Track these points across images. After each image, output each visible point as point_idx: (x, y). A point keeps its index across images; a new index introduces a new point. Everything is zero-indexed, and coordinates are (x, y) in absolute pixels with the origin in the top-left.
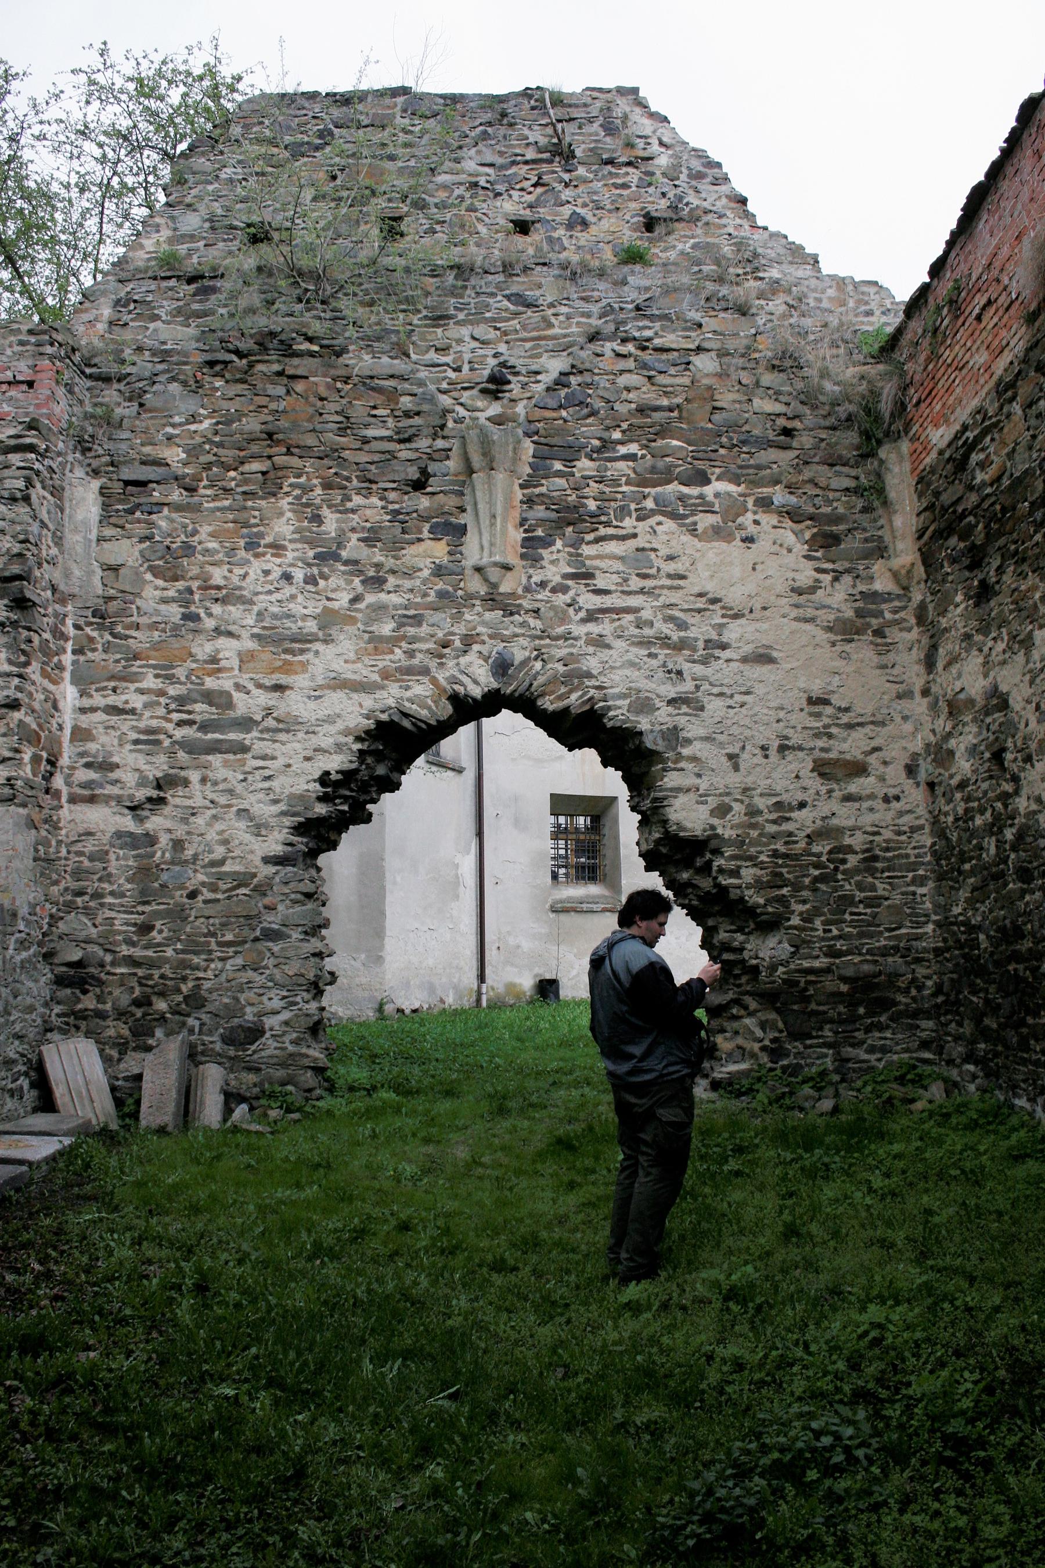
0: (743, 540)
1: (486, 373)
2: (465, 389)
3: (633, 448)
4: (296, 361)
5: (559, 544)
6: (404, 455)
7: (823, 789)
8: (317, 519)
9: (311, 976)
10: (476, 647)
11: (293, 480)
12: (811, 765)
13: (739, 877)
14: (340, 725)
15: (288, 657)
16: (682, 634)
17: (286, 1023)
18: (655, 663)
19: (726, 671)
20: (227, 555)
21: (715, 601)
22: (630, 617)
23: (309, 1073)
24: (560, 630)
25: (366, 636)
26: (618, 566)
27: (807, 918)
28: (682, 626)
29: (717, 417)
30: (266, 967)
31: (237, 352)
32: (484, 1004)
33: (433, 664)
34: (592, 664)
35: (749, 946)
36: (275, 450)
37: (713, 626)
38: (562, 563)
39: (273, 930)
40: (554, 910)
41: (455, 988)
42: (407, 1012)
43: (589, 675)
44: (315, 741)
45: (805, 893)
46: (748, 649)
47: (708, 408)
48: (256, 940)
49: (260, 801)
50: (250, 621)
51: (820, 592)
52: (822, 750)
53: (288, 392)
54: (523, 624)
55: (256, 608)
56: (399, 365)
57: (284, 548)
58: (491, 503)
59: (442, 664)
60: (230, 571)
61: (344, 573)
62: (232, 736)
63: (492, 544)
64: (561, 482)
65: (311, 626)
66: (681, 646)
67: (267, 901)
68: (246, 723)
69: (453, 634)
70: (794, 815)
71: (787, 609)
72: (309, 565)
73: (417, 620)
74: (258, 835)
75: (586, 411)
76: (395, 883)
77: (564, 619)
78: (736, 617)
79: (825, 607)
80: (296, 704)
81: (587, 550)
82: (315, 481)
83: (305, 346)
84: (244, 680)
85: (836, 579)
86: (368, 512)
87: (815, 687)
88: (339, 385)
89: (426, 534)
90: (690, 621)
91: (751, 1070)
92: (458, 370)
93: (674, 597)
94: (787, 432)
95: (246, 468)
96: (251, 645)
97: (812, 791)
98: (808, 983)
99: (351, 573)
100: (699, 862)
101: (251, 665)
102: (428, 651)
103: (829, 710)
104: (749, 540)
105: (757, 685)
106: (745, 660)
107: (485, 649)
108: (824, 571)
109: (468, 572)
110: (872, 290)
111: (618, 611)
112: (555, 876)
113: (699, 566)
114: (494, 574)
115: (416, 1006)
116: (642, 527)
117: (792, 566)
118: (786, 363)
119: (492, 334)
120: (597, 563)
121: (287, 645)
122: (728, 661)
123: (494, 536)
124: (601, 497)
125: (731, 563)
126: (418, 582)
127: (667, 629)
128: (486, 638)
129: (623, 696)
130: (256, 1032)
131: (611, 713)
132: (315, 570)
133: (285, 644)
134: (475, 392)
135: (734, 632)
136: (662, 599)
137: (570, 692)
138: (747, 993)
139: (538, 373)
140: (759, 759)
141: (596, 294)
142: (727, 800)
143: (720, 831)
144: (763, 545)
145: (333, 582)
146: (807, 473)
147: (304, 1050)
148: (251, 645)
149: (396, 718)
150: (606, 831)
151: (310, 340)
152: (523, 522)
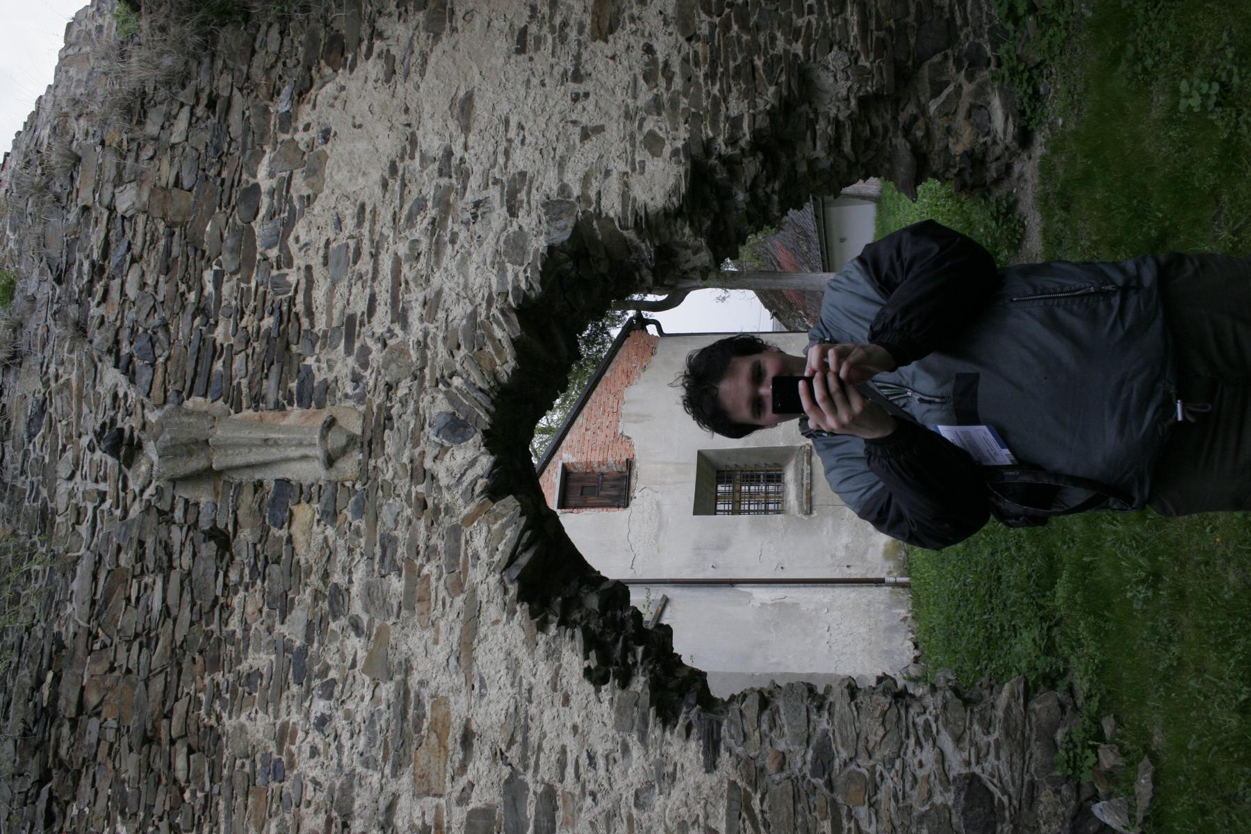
0: (326, 141)
1: (110, 460)
2: (125, 487)
3: (208, 276)
4: (62, 702)
5: (310, 361)
6: (186, 561)
7: (630, 27)
8: (253, 677)
9: (885, 701)
10: (428, 464)
11: (202, 712)
12: (600, 44)
13: (739, 118)
14: (521, 652)
15: (425, 725)
16: (430, 204)
17: (958, 740)
18: (463, 235)
19: (478, 149)
20: (286, 808)
21: (393, 169)
22: (405, 269)
23: (1035, 705)
25: (404, 613)
26: (342, 288)
27: (794, 34)
28: (421, 205)
29: (187, 183)
30: (872, 770)
31: (41, 782)
32: (906, 579)
33: (446, 521)
34: (459, 312)
35: (833, 112)
36: (163, 734)
38: (332, 356)
39: (815, 760)
40: (809, 512)
41: (890, 607)
42: (917, 653)
43: (473, 316)
44: (541, 690)
45: (762, 38)
46: (453, 125)
47: (175, 191)
48: (830, 785)
49: (625, 773)
50: (375, 778)
51: (393, 51)
52: (581, 32)
53: (98, 714)
55: (359, 769)
56: (84, 569)
57: (285, 726)
58: (250, 446)
59: (448, 510)
60: (309, 803)
61: (321, 644)
62: (531, 811)
63: (300, 444)
64: (239, 361)
65: (387, 690)
66: (444, 206)
67: (771, 767)
68: (513, 788)
69: (409, 493)
70: (661, 58)
71: (410, 86)
72: (309, 691)
73: (388, 543)
74: (673, 777)
75: (161, 335)
76: (778, 664)
77: (402, 351)
78: (413, 141)
79: (411, 44)
80: (490, 715)
81: (321, 325)
82: (207, 681)
83: (45, 690)
84: (454, 790)
85: (380, 35)
86: (250, 609)
87: (505, 46)
88: (97, 646)
89: (283, 533)
90: (415, 195)
91: (1001, 89)
92: (103, 496)
93: (385, 215)
94: (211, 105)
95: (181, 775)
96: (406, 779)
97: (632, 40)
98: (879, 28)
99: (323, 632)
100: (721, 174)
101: (433, 778)
102: (429, 528)
103: (533, 29)
104: (326, 135)
105: (498, 113)
106: (466, 129)
107: (431, 452)
109: (334, 475)
110: (76, 28)
111: (396, 282)
112: (778, 512)
113: (350, 189)
114: (336, 440)
115: (910, 644)
116: (299, 261)
117: (360, 83)
118: (136, 107)
119: (69, 455)
120: (336, 313)
121: (409, 726)
122: (466, 148)
123: (289, 443)
124: (259, 313)
125: (351, 153)
126: (341, 542)
127: (422, 223)
128: (417, 451)
129: (502, 271)
130: (973, 788)
131: (523, 286)
132: (316, 683)
133: (407, 729)
134: (130, 474)
135: (431, 144)
136: (386, 231)
137: (492, 337)
138: (895, 118)
139: (115, 396)
140: (590, 104)
141: (40, 332)
142: (639, 138)
143: (680, 144)
144: (334, 118)
145: (332, 659)
146: (257, 74)
147: (1000, 713)
148: (406, 779)
149: (515, 572)
150: (732, 464)
151: (40, 682)
152: (279, 407)
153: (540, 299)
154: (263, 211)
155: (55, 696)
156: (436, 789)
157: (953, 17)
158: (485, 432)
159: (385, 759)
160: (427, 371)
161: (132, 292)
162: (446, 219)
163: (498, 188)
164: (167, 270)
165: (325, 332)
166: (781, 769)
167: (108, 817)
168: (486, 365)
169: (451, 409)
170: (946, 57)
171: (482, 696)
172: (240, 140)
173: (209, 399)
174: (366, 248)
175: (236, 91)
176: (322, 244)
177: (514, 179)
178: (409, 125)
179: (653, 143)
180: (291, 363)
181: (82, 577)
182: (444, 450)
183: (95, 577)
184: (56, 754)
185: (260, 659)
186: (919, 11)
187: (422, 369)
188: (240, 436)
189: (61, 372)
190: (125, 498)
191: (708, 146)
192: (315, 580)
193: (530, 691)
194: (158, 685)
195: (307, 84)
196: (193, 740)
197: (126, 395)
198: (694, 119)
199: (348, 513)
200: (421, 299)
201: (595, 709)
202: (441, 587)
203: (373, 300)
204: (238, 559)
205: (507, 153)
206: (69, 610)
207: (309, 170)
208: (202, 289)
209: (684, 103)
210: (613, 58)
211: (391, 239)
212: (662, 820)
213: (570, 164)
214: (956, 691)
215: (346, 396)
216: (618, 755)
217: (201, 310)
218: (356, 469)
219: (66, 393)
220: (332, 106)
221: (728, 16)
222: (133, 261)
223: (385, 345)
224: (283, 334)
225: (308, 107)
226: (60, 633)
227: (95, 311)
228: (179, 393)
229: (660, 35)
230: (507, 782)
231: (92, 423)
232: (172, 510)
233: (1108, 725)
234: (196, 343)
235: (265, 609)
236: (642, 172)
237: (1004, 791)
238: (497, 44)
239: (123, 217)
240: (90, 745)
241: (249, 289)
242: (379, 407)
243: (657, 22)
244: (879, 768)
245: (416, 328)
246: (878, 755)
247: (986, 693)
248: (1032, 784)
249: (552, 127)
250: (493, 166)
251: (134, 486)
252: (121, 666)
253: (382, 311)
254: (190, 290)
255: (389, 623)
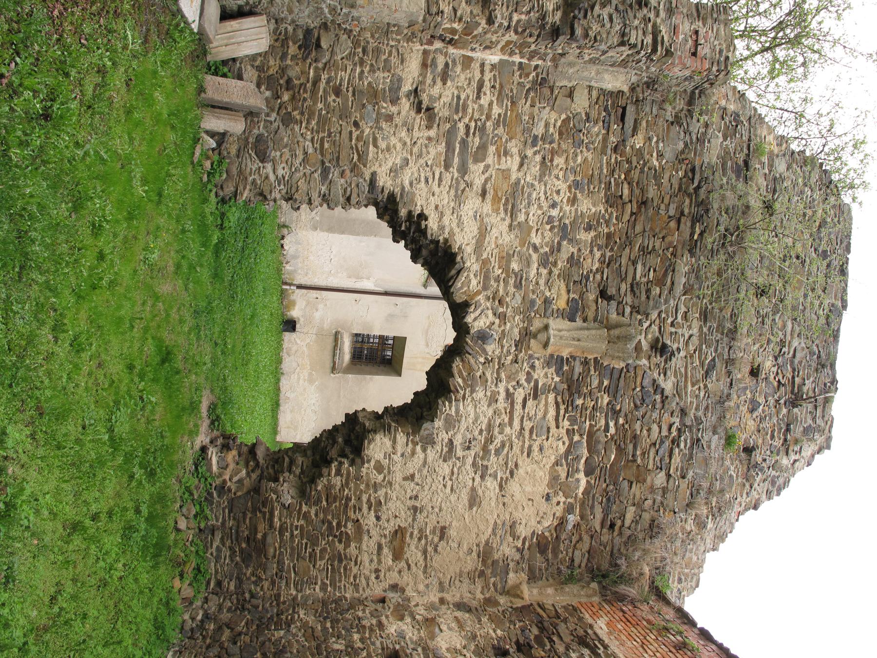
1: (668, 342)
3: (612, 430)
4: (689, 224)
5: (557, 379)
6: (623, 286)
7: (387, 532)
8: (589, 228)
9: (296, 196)
10: (497, 321)
14: (456, 230)
16: (493, 452)
17: (267, 177)
18: (476, 433)
20: (572, 168)
21: (512, 473)
22: (507, 420)
24: (503, 376)
26: (540, 415)
27: (306, 516)
28: (498, 452)
29: (626, 482)
30: (305, 168)
31: (699, 187)
32: (285, 287)
33: (489, 293)
34: (480, 394)
35: (291, 477)
36: (635, 206)
37: (496, 472)
38: (545, 380)
40: (337, 333)
41: (295, 271)
42: (282, 242)
44: (448, 212)
46: (480, 492)
48: (323, 163)
51: (511, 539)
52: (412, 533)
53: (670, 217)
54: (509, 352)
55: (536, 183)
56: (679, 289)
57: (573, 205)
59: (488, 298)
60: (561, 169)
61: (553, 241)
62: (456, 160)
64: (595, 383)
65: (521, 218)
67: (348, 172)
68: (463, 170)
69: (507, 308)
72: (560, 220)
73: (518, 286)
77: (509, 378)
80: (472, 204)
81: (551, 397)
82: (612, 229)
84: (492, 171)
85: (518, 550)
86: (590, 260)
87: (451, 532)
88: (671, 249)
89: (572, 296)
90: (501, 458)
92: (672, 325)
93: (516, 450)
94: (612, 526)
95: (626, 186)
96: (514, 177)
97: (386, 525)
98: (264, 513)
101: (501, 177)
103: (436, 539)
104: (548, 498)
106: (473, 489)
107: (495, 327)
108: (524, 543)
109: (545, 321)
110: (693, 584)
113: (535, 466)
114: (542, 337)
115: (285, 247)
120: (543, 402)
122: (473, 479)
126: (542, 288)
127: (497, 442)
128: (502, 328)
129: (457, 411)
131: (447, 403)
133: (511, 199)
134: (657, 334)
135: (491, 484)
136: (516, 441)
137: (463, 379)
138: (262, 472)
139: (665, 375)
141: (710, 415)
142: (386, 471)
143: (366, 465)
144: (544, 506)
145: (548, 234)
146: (586, 538)
147: (248, 187)
148: (514, 177)
149: (457, 266)
150: (382, 368)
152: (574, 358)
153: (440, 397)
154: (583, 461)
155: (693, 227)
156: (500, 172)
157: (229, 513)
158: (469, 333)
159: (523, 187)
160: (497, 367)
161: (655, 427)
162: (485, 443)
163: (458, 455)
164: (635, 437)
165: (549, 392)
166: (343, 171)
167: (663, 169)
168: (467, 366)
169: (485, 346)
170: (235, 494)
171: (476, 212)
172: (596, 503)
173: (612, 366)
174: (527, 434)
175: (599, 531)
176: (550, 439)
177: (450, 458)
178: (503, 496)
179: (379, 468)
180: (567, 379)
181: (679, 284)
182: (489, 327)
183: (673, 283)
184: (691, 201)
185: (586, 237)
186: (244, 519)
187: (499, 368)
188: (591, 342)
189: (697, 392)
190: (660, 322)
191: (352, 463)
192: (556, 272)
193: (453, 212)
194: (638, 228)
195: (558, 528)
196: (619, 201)
197: (659, 375)
198: (358, 478)
199: (539, 302)
200: (498, 403)
201: (424, 202)
202: (493, 263)
203: (524, 407)
204: (596, 285)
205: (453, 473)
206: (686, 268)
207: (557, 480)
208: (616, 424)
209: (362, 487)
210: (396, 516)
211: (514, 436)
212: (397, 153)
213: (421, 463)
214: (265, 198)
215: (538, 359)
216: (415, 182)
217: (616, 413)
218: (534, 323)
219: (694, 380)
220: (545, 513)
221: (337, 530)
222: (655, 444)
223: (518, 382)
224: (571, 395)
225: (558, 514)
226: (691, 257)
227: (677, 420)
228: (628, 371)
229: (372, 525)
230: (466, 173)
231: (677, 362)
232: (631, 312)
233: (205, 178)
234: (619, 396)
235: (582, 260)
236: (385, 453)
237: (250, 155)
238: (455, 534)
239: (661, 469)
240: (673, 203)
241: (590, 420)
242: (521, 352)
243: (373, 532)
244: (301, 168)
245: (501, 389)
246: (302, 173)
247: (252, 199)
248: (238, 157)
249: (429, 484)
250: (460, 467)
251: (655, 328)
252: (658, 238)
253: (519, 399)
254: (623, 425)
255: (519, 248)
